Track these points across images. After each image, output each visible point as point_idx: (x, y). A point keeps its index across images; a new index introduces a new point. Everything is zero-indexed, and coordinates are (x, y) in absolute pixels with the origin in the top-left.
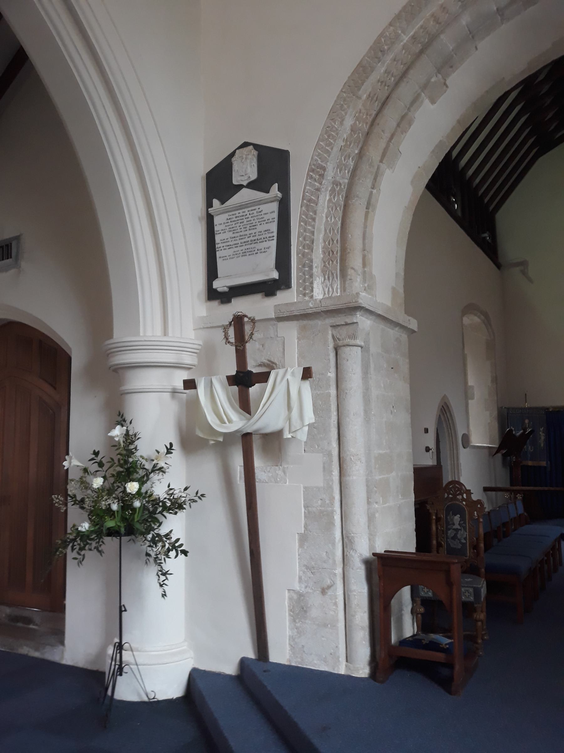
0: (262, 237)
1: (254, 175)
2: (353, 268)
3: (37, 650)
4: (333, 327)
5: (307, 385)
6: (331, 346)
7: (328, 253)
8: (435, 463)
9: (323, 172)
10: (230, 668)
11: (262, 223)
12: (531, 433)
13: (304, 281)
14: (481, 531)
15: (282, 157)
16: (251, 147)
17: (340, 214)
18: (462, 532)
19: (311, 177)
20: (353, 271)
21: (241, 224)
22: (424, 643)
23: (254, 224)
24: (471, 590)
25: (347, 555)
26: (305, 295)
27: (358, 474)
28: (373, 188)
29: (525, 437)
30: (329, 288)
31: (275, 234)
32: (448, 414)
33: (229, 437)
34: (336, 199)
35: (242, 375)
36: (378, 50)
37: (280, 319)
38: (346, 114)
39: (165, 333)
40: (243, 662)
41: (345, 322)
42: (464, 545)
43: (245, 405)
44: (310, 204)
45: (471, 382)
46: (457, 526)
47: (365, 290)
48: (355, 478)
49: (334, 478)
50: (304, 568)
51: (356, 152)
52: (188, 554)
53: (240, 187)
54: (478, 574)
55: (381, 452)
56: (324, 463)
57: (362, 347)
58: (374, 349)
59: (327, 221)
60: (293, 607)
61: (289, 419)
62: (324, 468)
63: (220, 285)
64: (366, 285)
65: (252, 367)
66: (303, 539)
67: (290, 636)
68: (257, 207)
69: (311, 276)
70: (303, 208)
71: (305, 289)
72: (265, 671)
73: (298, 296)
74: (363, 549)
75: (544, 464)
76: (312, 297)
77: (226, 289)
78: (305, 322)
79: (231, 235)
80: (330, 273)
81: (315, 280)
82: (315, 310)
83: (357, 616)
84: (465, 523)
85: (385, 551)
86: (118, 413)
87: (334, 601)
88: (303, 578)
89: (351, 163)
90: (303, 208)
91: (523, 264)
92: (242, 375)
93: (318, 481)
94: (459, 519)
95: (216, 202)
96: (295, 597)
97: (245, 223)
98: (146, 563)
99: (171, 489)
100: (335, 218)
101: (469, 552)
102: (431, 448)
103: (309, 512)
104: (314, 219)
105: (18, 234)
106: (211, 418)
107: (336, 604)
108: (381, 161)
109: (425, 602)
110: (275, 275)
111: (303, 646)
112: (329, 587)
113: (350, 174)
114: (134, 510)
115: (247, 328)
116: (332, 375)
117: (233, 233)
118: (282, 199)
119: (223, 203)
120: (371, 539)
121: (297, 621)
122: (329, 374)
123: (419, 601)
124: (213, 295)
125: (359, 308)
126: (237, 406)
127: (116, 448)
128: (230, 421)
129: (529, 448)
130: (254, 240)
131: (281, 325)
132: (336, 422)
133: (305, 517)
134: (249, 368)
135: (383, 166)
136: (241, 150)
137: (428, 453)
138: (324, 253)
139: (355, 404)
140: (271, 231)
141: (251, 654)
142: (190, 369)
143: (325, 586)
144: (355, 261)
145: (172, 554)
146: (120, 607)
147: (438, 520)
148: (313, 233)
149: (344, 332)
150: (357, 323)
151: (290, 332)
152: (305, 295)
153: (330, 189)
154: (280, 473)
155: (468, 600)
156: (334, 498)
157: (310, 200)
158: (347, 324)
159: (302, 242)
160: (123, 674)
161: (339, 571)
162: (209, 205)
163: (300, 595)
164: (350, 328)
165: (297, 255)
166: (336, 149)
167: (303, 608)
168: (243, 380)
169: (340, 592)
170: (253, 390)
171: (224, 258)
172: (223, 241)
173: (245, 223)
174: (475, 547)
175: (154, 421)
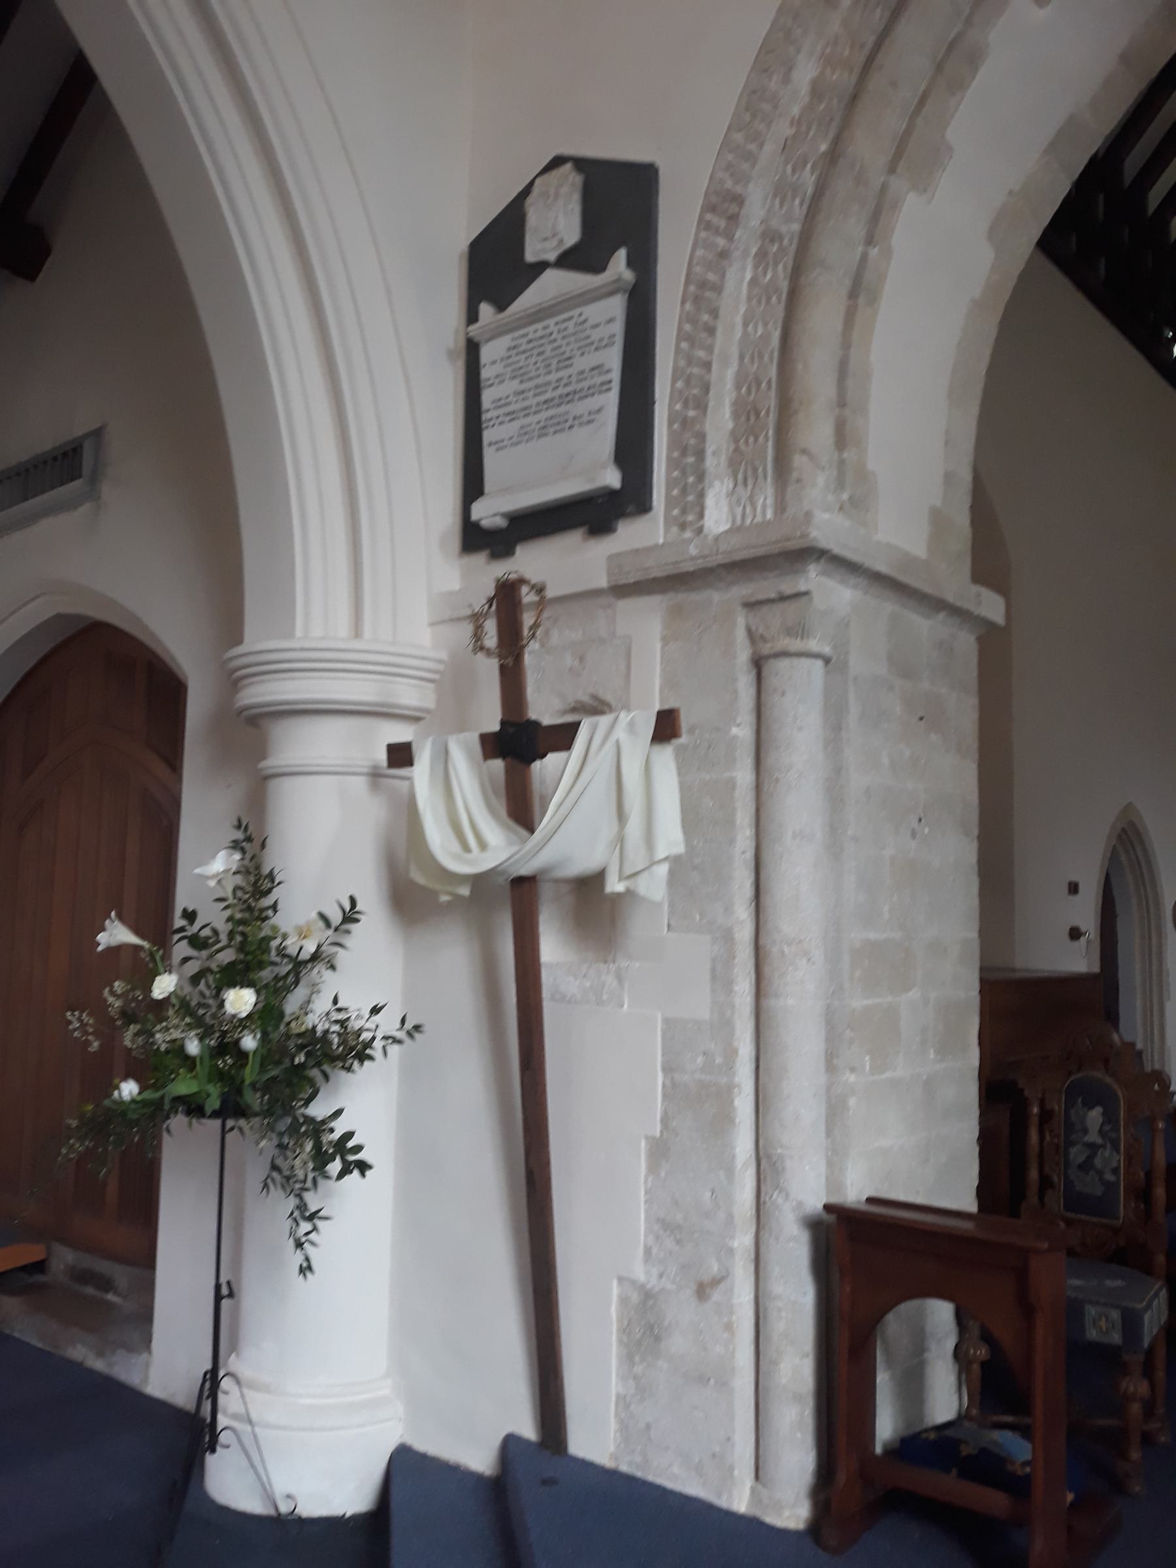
0: (585, 384)
2: (804, 451)
3: (100, 1354)
5: (665, 756)
6: (743, 655)
7: (746, 412)
8: (1096, 969)
9: (737, 209)
10: (480, 1459)
11: (587, 349)
13: (684, 492)
14: (1160, 1157)
16: (568, 166)
17: (779, 311)
18: (1107, 1153)
19: (708, 226)
20: (805, 459)
21: (541, 358)
22: (964, 1453)
23: (567, 355)
24: (1115, 1315)
25: (765, 1203)
26: (683, 526)
28: (870, 241)
30: (744, 507)
31: (616, 376)
32: (1138, 849)
34: (768, 277)
35: (511, 730)
37: (621, 591)
38: (798, 51)
39: (357, 632)
40: (510, 1444)
41: (779, 593)
42: (1111, 1187)
43: (521, 809)
44: (703, 295)
46: (1093, 1137)
47: (841, 509)
48: (790, 1002)
49: (737, 1001)
50: (656, 1227)
51: (823, 147)
52: (368, 1173)
53: (542, 266)
54: (1149, 1271)
55: (872, 936)
56: (714, 960)
57: (827, 661)
58: (858, 664)
59: (745, 334)
60: (630, 1321)
61: (620, 840)
62: (713, 970)
63: (487, 512)
64: (845, 496)
65: (543, 709)
66: (659, 1151)
67: (618, 1396)
68: (576, 312)
69: (701, 476)
70: (688, 306)
71: (684, 512)
72: (546, 1482)
73: (667, 531)
74: (808, 1189)
76: (700, 531)
77: (501, 522)
78: (681, 597)
79: (515, 385)
80: (750, 472)
81: (711, 485)
82: (700, 563)
83: (782, 1366)
84: (1116, 1129)
85: (870, 1200)
86: (236, 823)
87: (725, 1320)
88: (655, 1251)
89: (808, 179)
90: (688, 306)
92: (511, 730)
94: (1101, 1120)
95: (486, 310)
96: (635, 1297)
97: (548, 353)
98: (266, 1186)
99: (339, 1010)
100: (765, 325)
101: (1124, 1209)
102: (1083, 929)
103: (674, 1085)
104: (711, 331)
105: (98, 425)
107: (729, 1327)
108: (892, 170)
110: (612, 478)
111: (648, 1427)
112: (716, 1282)
113: (805, 206)
114: (242, 1055)
116: (743, 732)
117: (521, 382)
118: (635, 286)
119: (501, 307)
121: (637, 1359)
122: (734, 730)
124: (475, 539)
125: (804, 554)
127: (224, 904)
128: (483, 845)
130: (568, 394)
131: (626, 606)
132: (750, 854)
133: (664, 1095)
134: (533, 715)
135: (897, 184)
136: (546, 176)
137: (1076, 944)
138: (736, 415)
139: (800, 808)
140: (606, 368)
141: (528, 1430)
142: (418, 719)
143: (706, 1278)
144: (816, 432)
145: (335, 1167)
146: (218, 1287)
147: (1046, 1116)
148: (707, 366)
149: (774, 618)
150: (806, 593)
151: (645, 623)
152: (683, 526)
153: (754, 250)
154: (610, 980)
155: (1105, 1340)
156: (735, 1052)
157: (703, 285)
158: (783, 598)
159: (681, 392)
160: (218, 1448)
161: (743, 1241)
162: (472, 317)
163: (648, 1297)
164: (791, 607)
165: (671, 423)
167: (652, 1328)
168: (519, 744)
171: (499, 445)
173: (548, 353)
174: (1144, 1194)
175: (325, 846)
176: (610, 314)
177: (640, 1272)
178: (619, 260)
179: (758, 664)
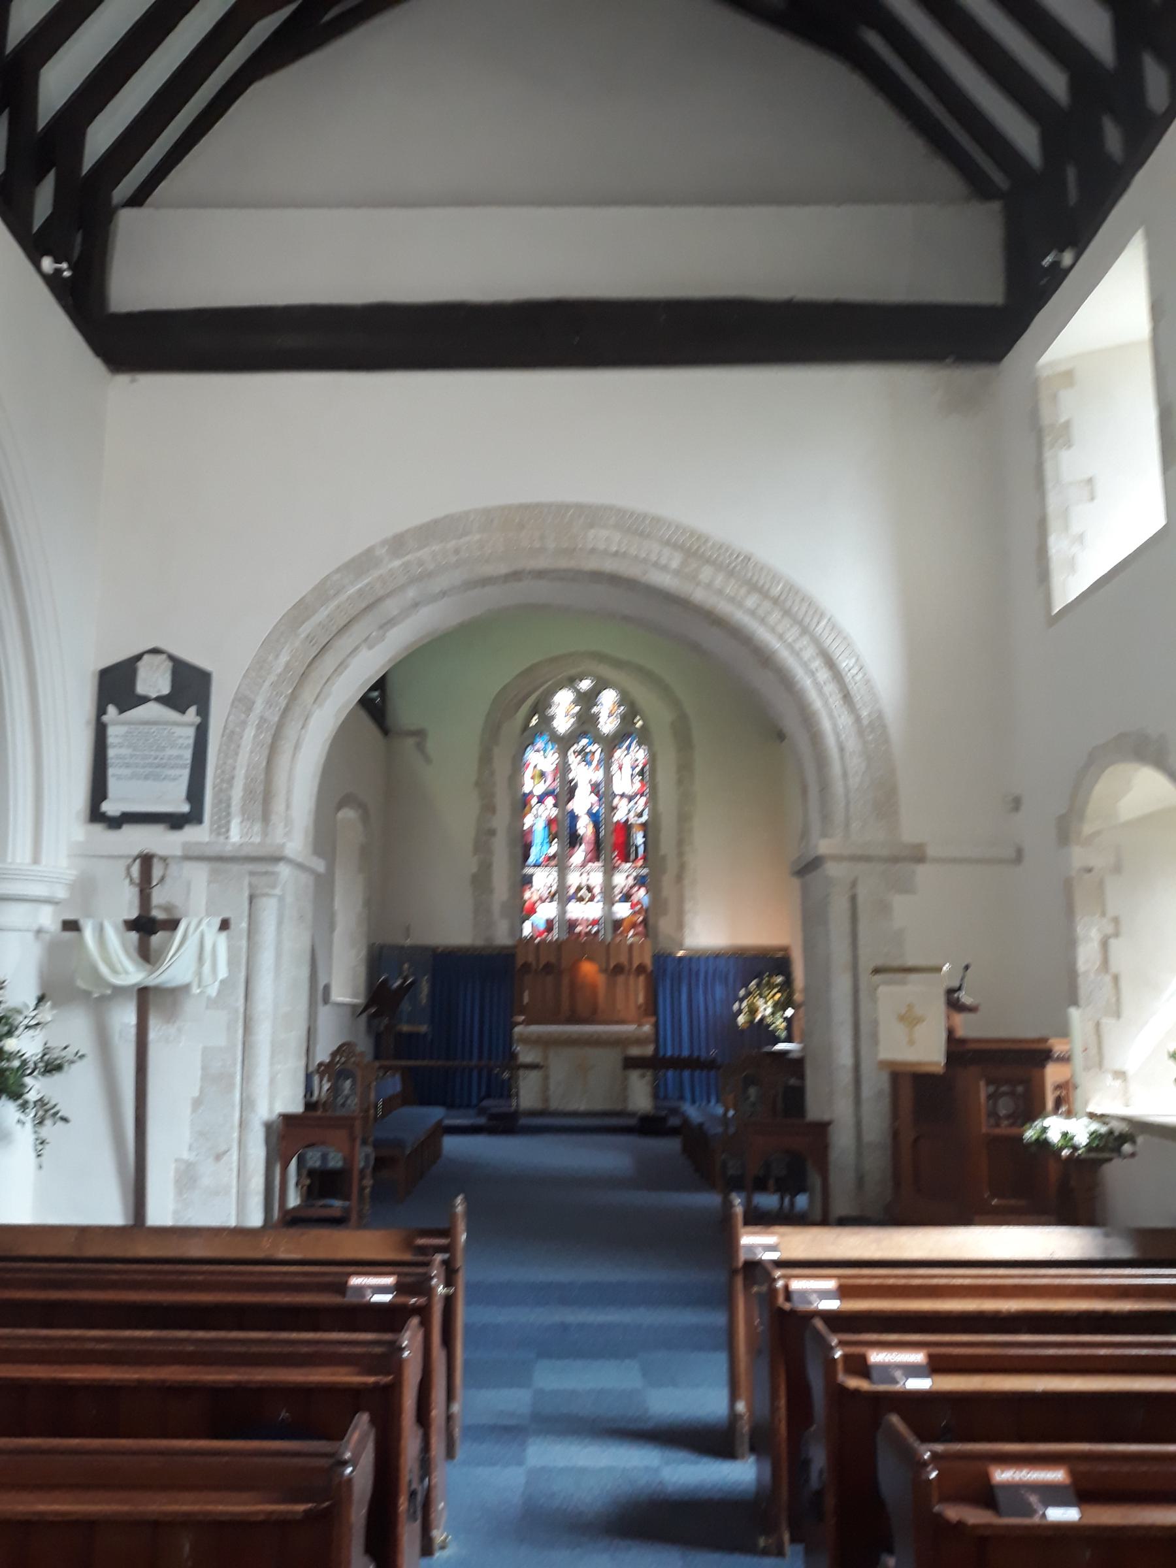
1: (165, 689)
4: (252, 874)
5: (224, 935)
6: (246, 894)
7: (249, 792)
12: (412, 984)
15: (203, 678)
16: (164, 657)
26: (219, 834)
27: (264, 1033)
29: (404, 990)
33: (119, 991)
36: (322, 592)
37: (187, 858)
39: (36, 860)
43: (146, 955)
44: (232, 738)
45: (336, 907)
61: (199, 973)
63: (110, 807)
65: (158, 914)
66: (197, 1103)
69: (229, 814)
75: (423, 1029)
79: (129, 751)
91: (420, 734)
93: (221, 1041)
95: (112, 710)
106: (104, 969)
107: (231, 1170)
109: (311, 1173)
110: (185, 808)
115: (157, 871)
120: (272, 1099)
123: (305, 1172)
124: (96, 815)
126: (135, 955)
128: (127, 973)
129: (406, 1006)
139: (266, 958)
151: (198, 874)
161: (236, 1135)
162: (101, 711)
166: (267, 684)
168: (148, 927)
169: (235, 1157)
170: (156, 939)
171: (119, 778)
172: (118, 757)
176: (188, 735)
177: (185, 1155)
178: (192, 710)
179: (251, 898)
